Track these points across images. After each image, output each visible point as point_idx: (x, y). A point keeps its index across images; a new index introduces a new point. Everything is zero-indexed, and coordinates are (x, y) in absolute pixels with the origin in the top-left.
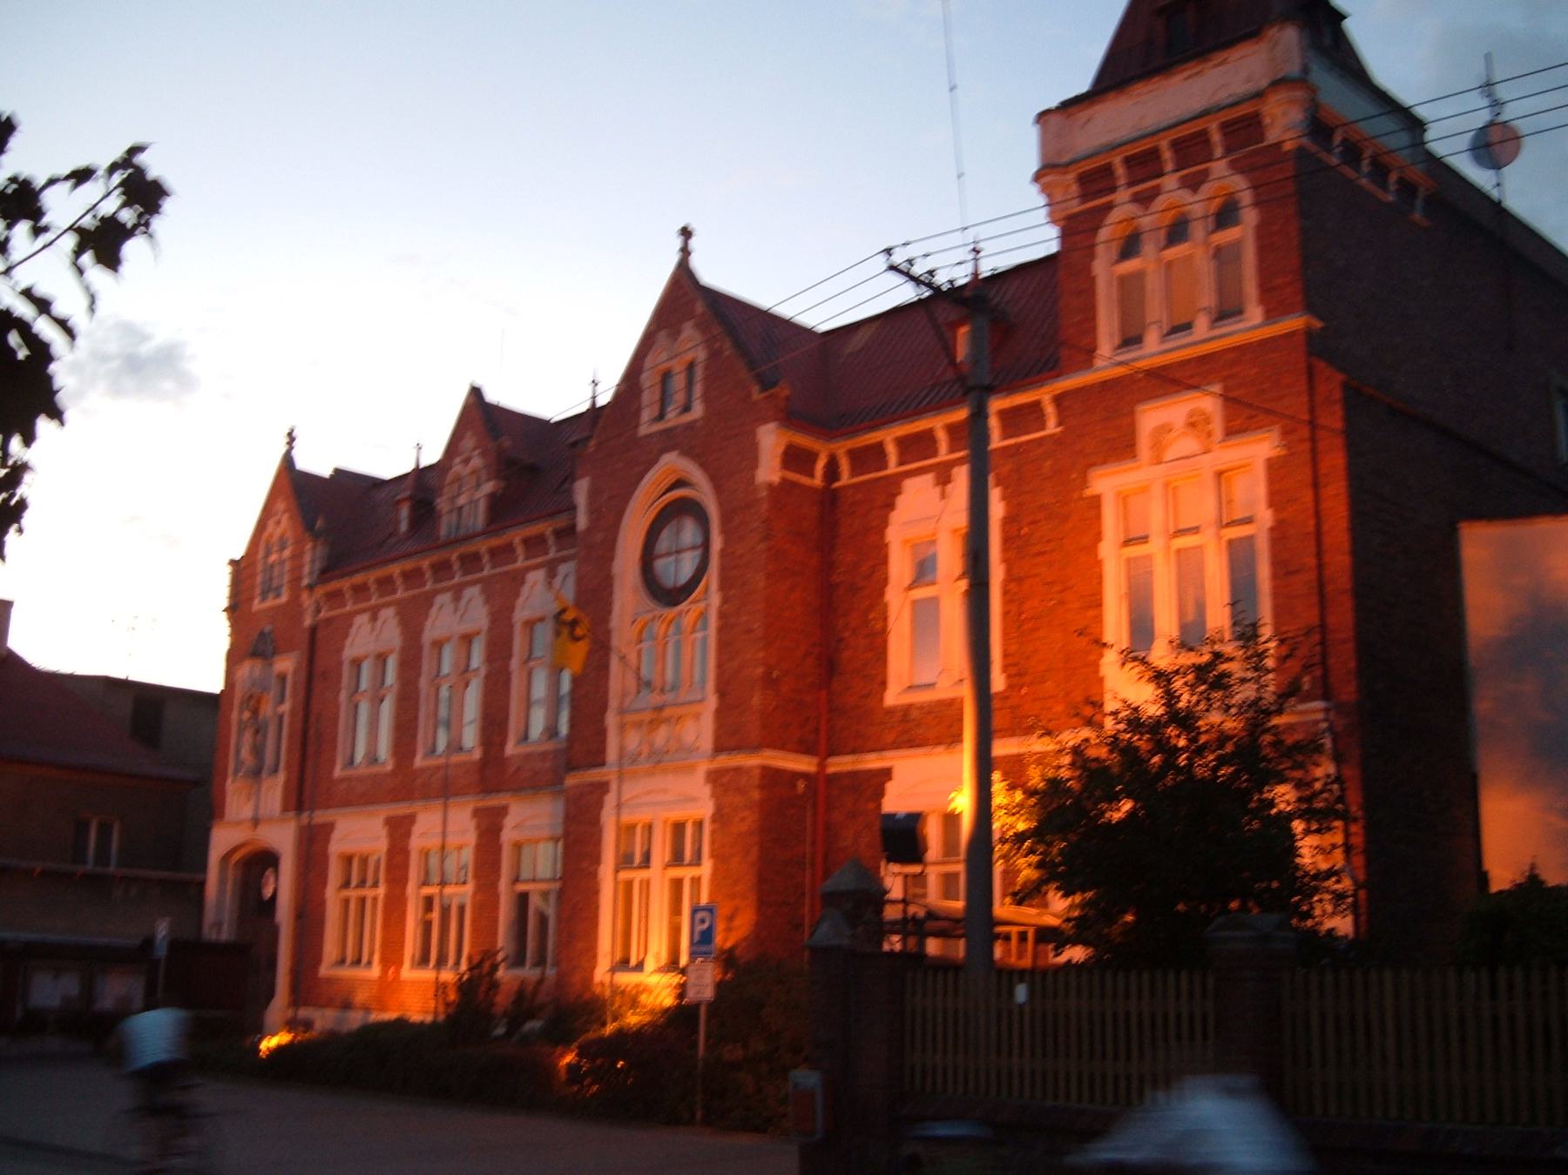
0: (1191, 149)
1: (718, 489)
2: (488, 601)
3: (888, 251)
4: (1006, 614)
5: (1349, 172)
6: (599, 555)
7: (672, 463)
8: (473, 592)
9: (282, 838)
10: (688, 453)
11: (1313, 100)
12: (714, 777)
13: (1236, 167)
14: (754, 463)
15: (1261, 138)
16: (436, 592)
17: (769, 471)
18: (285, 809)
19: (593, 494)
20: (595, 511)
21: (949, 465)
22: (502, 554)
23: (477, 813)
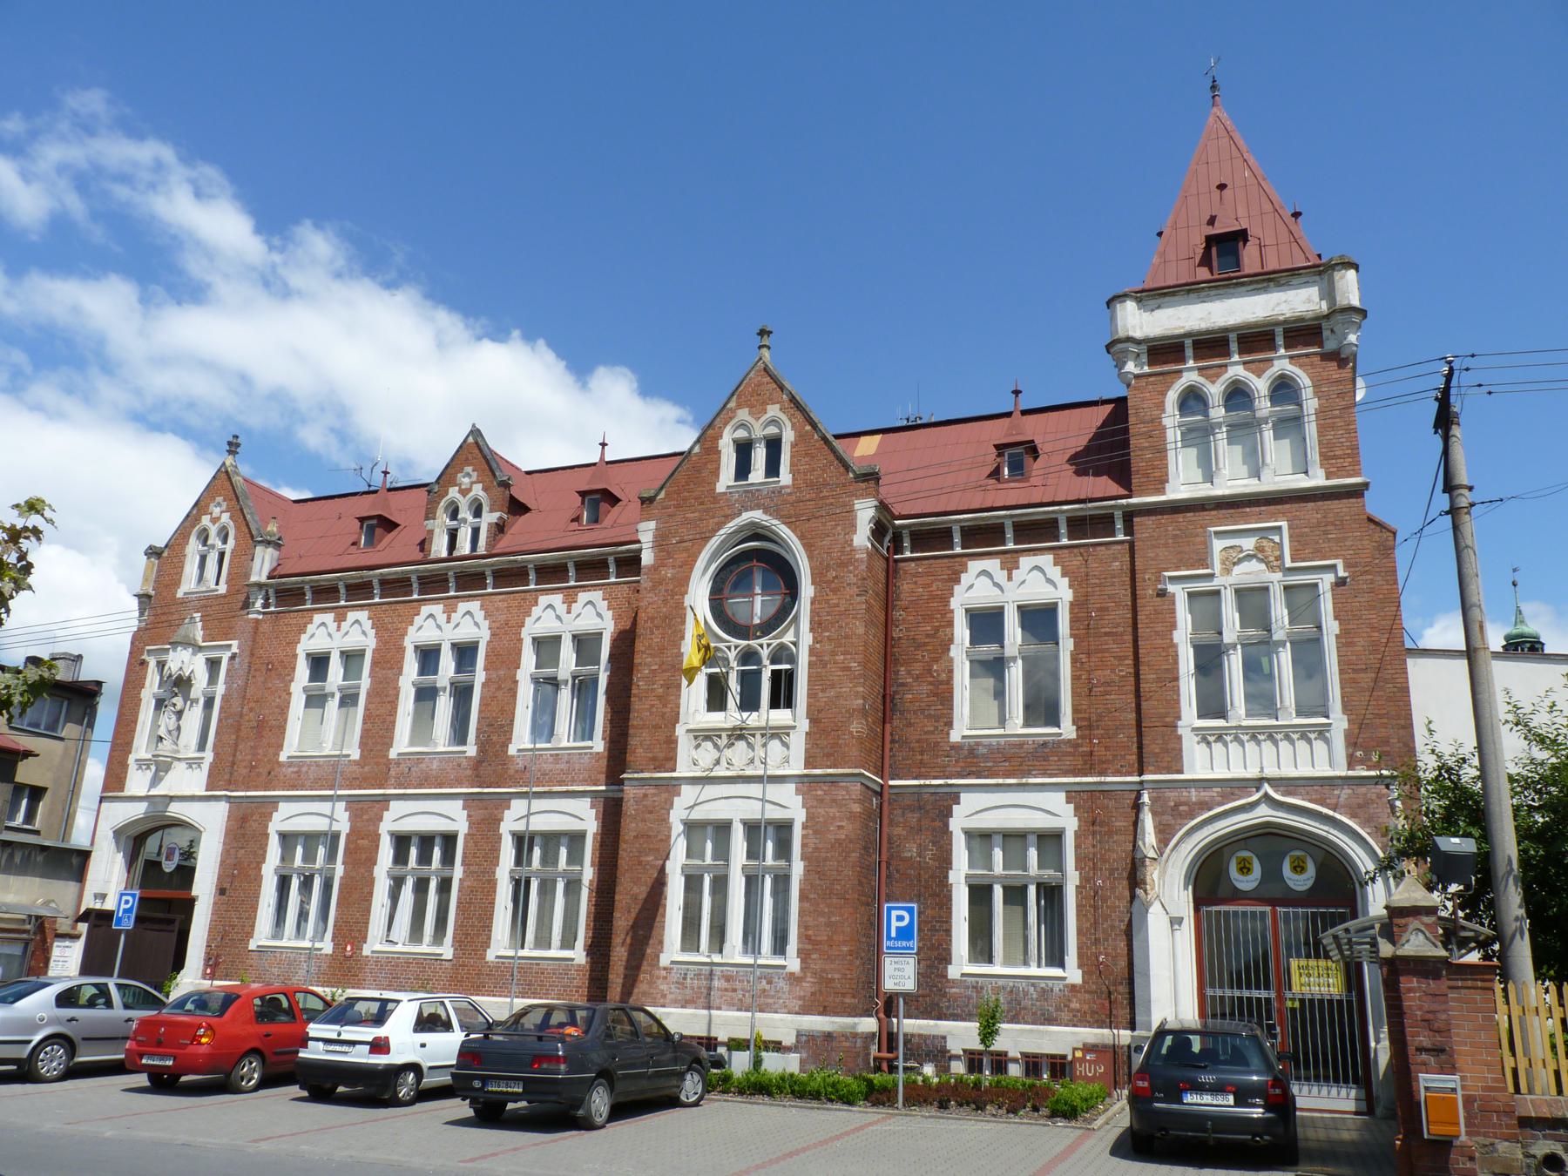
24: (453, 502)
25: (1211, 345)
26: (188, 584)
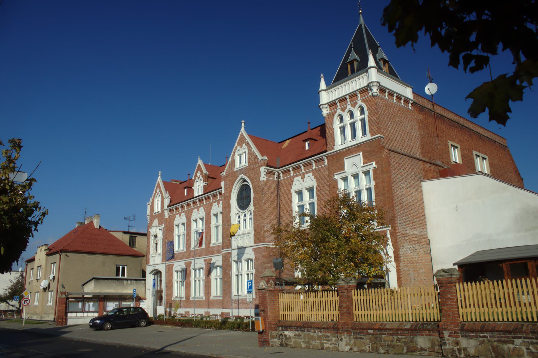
0: (353, 95)
1: (252, 183)
2: (205, 211)
3: (44, 214)
4: (318, 208)
5: (391, 100)
6: (227, 199)
7: (242, 176)
8: (202, 209)
9: (162, 268)
10: (245, 174)
11: (380, 85)
12: (254, 250)
13: (363, 101)
14: (260, 176)
15: (333, 149)
16: (193, 209)
17: (263, 177)
18: (162, 261)
19: (225, 185)
20: (225, 189)
21: (304, 174)
22: (208, 198)
23: (205, 261)
24: (340, 115)
25: (343, 100)
26: (156, 210)
